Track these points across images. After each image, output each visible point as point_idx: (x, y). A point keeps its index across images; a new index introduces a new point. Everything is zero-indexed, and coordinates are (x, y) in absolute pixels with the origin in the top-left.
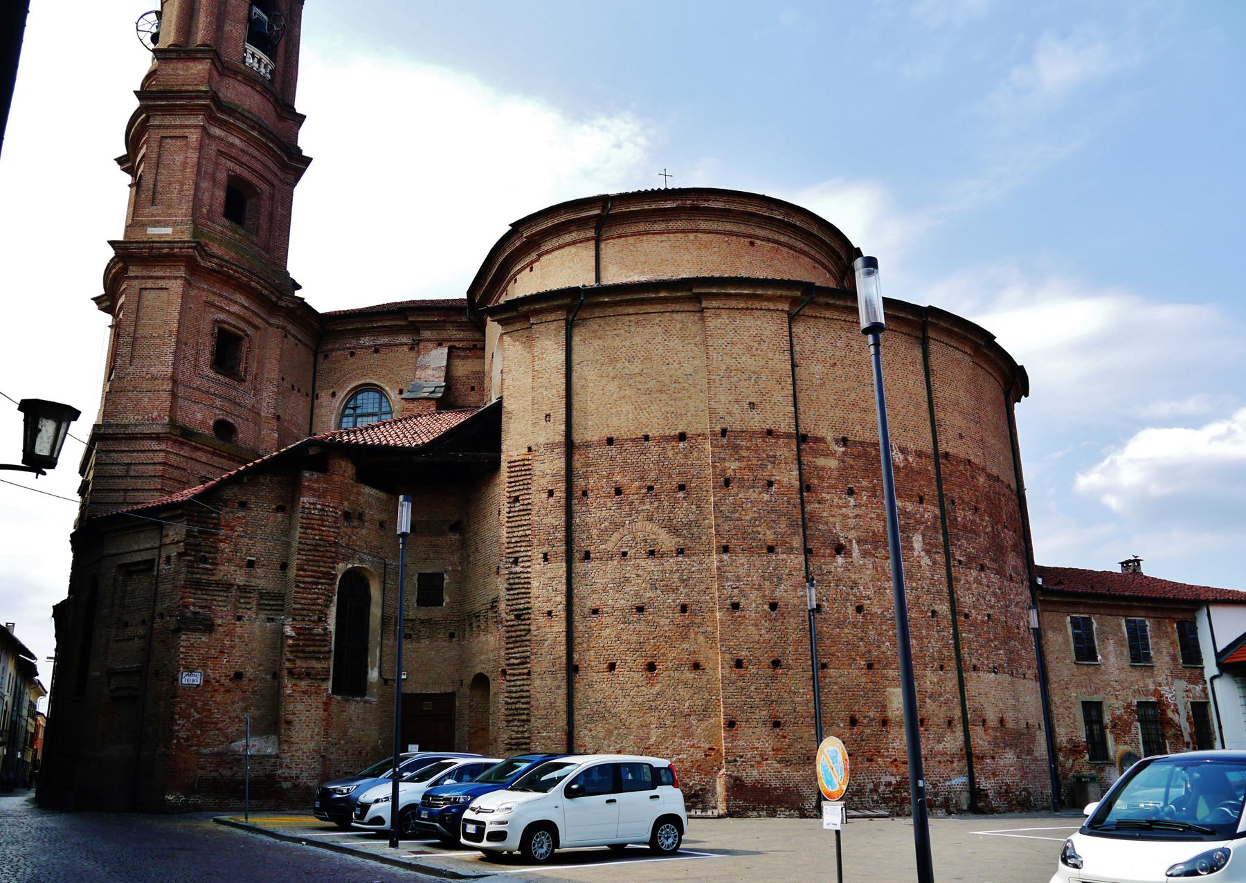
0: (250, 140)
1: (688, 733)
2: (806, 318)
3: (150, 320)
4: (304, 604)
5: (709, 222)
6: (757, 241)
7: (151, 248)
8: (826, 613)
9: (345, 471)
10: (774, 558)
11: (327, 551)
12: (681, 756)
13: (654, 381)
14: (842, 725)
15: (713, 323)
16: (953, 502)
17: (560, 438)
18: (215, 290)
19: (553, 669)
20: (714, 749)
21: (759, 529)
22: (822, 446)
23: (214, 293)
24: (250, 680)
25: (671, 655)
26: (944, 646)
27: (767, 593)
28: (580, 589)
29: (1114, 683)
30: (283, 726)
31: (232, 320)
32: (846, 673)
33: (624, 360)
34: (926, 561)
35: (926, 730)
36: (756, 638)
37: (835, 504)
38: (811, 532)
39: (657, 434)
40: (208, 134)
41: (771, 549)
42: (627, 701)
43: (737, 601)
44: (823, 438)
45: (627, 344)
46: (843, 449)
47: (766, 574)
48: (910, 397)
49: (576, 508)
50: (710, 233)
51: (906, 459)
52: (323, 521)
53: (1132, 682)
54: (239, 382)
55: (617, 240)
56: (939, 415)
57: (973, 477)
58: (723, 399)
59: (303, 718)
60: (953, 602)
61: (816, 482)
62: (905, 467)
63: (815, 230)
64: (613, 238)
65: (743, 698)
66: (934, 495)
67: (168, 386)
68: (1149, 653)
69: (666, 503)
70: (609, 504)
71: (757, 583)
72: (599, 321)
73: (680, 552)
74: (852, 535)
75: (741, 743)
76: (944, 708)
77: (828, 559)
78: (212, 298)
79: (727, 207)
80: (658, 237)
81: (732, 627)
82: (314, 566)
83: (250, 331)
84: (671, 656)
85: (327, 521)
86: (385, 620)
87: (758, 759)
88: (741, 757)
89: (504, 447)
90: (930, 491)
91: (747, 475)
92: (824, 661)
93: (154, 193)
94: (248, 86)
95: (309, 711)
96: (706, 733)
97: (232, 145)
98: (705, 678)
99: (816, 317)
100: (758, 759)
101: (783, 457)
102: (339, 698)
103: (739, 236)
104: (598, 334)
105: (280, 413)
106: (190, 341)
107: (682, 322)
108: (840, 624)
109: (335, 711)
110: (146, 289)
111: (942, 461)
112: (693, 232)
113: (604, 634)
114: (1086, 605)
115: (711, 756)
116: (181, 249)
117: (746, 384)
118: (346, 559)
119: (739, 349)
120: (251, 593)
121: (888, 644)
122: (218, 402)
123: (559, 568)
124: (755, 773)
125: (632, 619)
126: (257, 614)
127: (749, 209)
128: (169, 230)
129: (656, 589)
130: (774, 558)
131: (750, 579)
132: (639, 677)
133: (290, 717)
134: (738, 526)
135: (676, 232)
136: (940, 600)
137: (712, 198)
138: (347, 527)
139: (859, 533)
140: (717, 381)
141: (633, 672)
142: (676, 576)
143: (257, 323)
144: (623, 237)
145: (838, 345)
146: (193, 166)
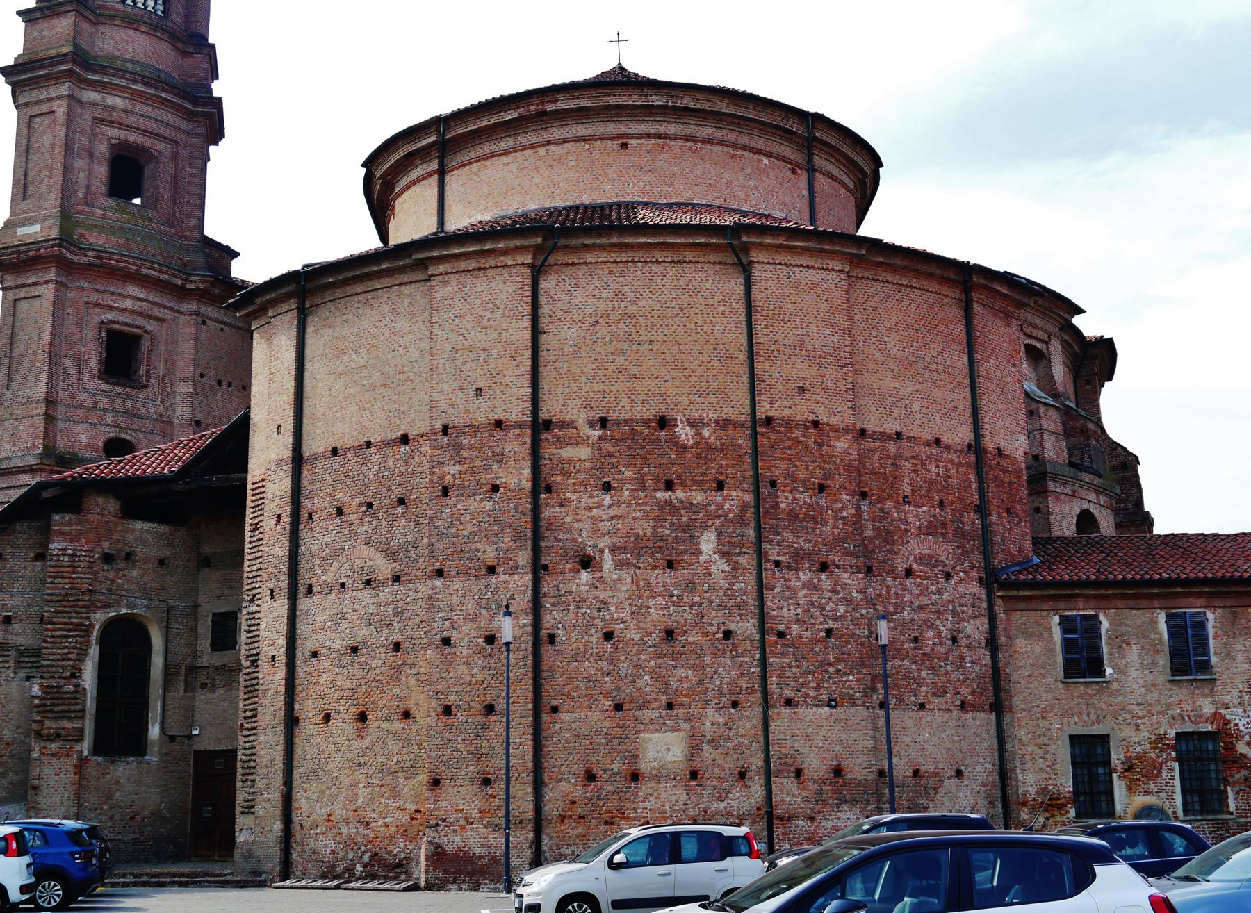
0: (135, 96)
1: (395, 794)
2: (559, 268)
3: (25, 334)
4: (52, 660)
5: (565, 128)
6: (632, 141)
7: (19, 253)
8: (562, 644)
9: (103, 509)
10: (494, 580)
11: (79, 600)
12: (386, 820)
13: (379, 374)
14: (573, 781)
15: (441, 292)
16: (773, 484)
17: (288, 453)
18: (98, 286)
19: (274, 723)
20: (420, 811)
21: (478, 546)
22: (570, 432)
23: (97, 291)
24: (8, 744)
25: (382, 703)
26: (742, 675)
27: (482, 624)
28: (303, 629)
29: (1135, 707)
30: (30, 792)
31: (125, 318)
32: (583, 717)
33: (351, 352)
34: (720, 565)
35: (698, 785)
36: (468, 678)
37: (583, 504)
38: (548, 544)
39: (379, 439)
40: (80, 102)
41: (492, 570)
42: (338, 757)
43: (448, 636)
44: (573, 422)
45: (355, 331)
46: (599, 433)
47: (484, 601)
48: (715, 349)
49: (302, 534)
50: (565, 142)
51: (699, 434)
52: (74, 567)
53: (1170, 704)
54: (139, 389)
55: (461, 169)
56: (759, 367)
57: (820, 445)
58: (446, 387)
59: (52, 783)
60: (762, 616)
61: (558, 479)
62: (696, 445)
63: (724, 107)
64: (457, 168)
65: (449, 750)
66: (744, 477)
67: (41, 409)
68: (1208, 661)
69: (384, 522)
70: (331, 527)
71: (471, 612)
72: (329, 305)
73: (396, 579)
74: (604, 542)
75: (444, 804)
76: (732, 756)
77: (568, 576)
78: (95, 297)
79: (582, 104)
80: (504, 159)
81: (441, 666)
82: (64, 618)
83: (150, 326)
84: (380, 704)
85: (79, 566)
86: (169, 672)
87: (463, 823)
88: (444, 820)
89: (250, 466)
90: (739, 471)
91: (469, 481)
92: (554, 703)
93: (25, 185)
94: (130, 28)
95: (58, 775)
96: (412, 793)
97: (111, 108)
98: (414, 728)
99: (573, 264)
100: (463, 823)
101: (512, 453)
102: (100, 759)
103: (604, 139)
104: (329, 321)
105: (201, 416)
106: (71, 352)
107: (411, 295)
108: (579, 657)
109: (94, 773)
110: (19, 299)
111: (760, 429)
112: (544, 145)
113: (321, 680)
114: (1088, 598)
115: (417, 819)
116: (46, 249)
117: (473, 365)
118: (106, 606)
119: (467, 322)
120: (9, 650)
121: (647, 677)
122: (109, 418)
123: (282, 605)
124: (457, 839)
125: (345, 662)
126: (15, 673)
127: (612, 101)
128: (36, 228)
129: (370, 625)
130: (494, 580)
131: (464, 608)
132: (349, 729)
133: (36, 782)
134: (454, 544)
135: (524, 149)
136: (741, 615)
137: (560, 97)
138: (108, 571)
139: (615, 540)
140: (440, 366)
141: (343, 726)
142: (391, 608)
143: (160, 315)
144: (466, 165)
145: (604, 295)
146: (60, 146)
